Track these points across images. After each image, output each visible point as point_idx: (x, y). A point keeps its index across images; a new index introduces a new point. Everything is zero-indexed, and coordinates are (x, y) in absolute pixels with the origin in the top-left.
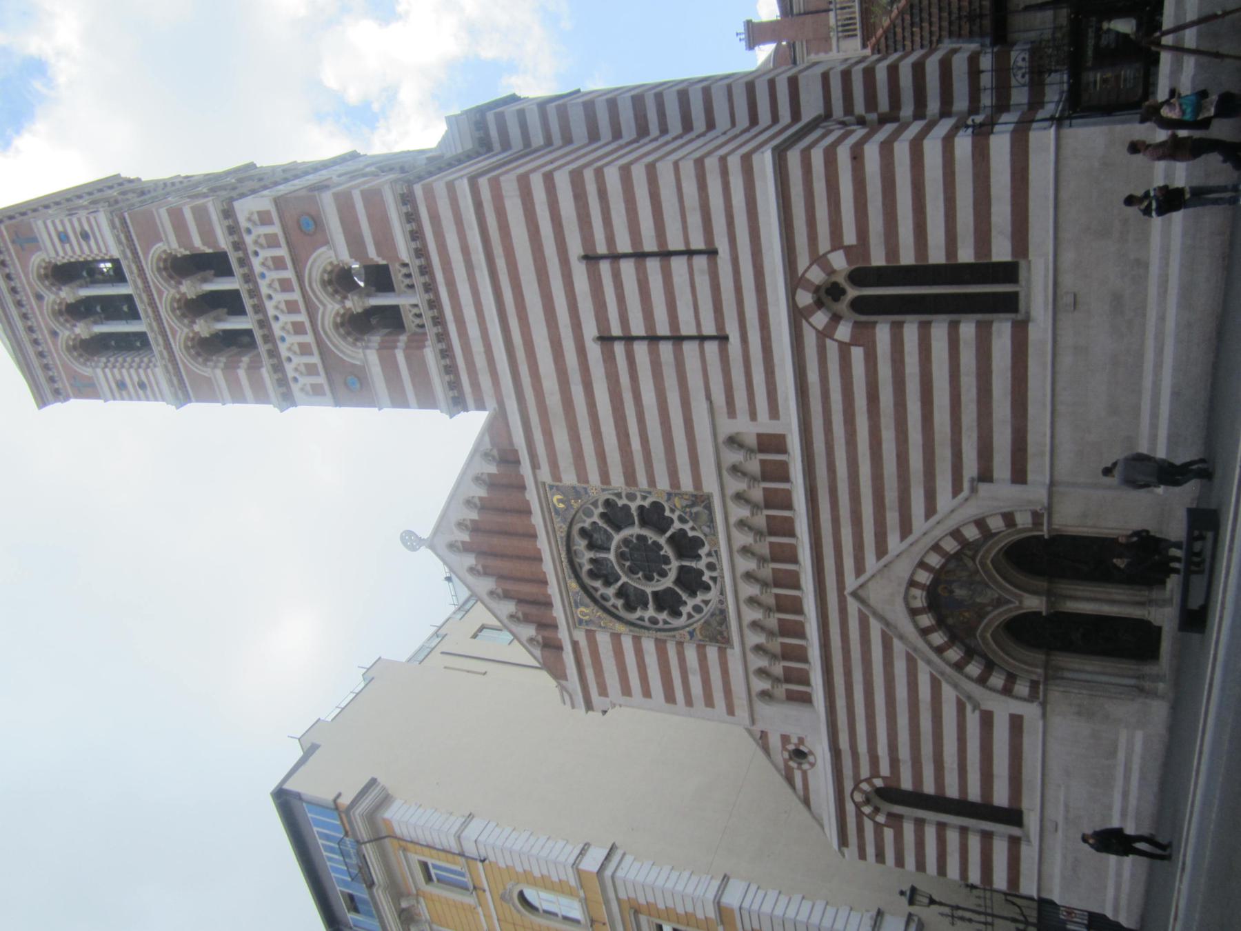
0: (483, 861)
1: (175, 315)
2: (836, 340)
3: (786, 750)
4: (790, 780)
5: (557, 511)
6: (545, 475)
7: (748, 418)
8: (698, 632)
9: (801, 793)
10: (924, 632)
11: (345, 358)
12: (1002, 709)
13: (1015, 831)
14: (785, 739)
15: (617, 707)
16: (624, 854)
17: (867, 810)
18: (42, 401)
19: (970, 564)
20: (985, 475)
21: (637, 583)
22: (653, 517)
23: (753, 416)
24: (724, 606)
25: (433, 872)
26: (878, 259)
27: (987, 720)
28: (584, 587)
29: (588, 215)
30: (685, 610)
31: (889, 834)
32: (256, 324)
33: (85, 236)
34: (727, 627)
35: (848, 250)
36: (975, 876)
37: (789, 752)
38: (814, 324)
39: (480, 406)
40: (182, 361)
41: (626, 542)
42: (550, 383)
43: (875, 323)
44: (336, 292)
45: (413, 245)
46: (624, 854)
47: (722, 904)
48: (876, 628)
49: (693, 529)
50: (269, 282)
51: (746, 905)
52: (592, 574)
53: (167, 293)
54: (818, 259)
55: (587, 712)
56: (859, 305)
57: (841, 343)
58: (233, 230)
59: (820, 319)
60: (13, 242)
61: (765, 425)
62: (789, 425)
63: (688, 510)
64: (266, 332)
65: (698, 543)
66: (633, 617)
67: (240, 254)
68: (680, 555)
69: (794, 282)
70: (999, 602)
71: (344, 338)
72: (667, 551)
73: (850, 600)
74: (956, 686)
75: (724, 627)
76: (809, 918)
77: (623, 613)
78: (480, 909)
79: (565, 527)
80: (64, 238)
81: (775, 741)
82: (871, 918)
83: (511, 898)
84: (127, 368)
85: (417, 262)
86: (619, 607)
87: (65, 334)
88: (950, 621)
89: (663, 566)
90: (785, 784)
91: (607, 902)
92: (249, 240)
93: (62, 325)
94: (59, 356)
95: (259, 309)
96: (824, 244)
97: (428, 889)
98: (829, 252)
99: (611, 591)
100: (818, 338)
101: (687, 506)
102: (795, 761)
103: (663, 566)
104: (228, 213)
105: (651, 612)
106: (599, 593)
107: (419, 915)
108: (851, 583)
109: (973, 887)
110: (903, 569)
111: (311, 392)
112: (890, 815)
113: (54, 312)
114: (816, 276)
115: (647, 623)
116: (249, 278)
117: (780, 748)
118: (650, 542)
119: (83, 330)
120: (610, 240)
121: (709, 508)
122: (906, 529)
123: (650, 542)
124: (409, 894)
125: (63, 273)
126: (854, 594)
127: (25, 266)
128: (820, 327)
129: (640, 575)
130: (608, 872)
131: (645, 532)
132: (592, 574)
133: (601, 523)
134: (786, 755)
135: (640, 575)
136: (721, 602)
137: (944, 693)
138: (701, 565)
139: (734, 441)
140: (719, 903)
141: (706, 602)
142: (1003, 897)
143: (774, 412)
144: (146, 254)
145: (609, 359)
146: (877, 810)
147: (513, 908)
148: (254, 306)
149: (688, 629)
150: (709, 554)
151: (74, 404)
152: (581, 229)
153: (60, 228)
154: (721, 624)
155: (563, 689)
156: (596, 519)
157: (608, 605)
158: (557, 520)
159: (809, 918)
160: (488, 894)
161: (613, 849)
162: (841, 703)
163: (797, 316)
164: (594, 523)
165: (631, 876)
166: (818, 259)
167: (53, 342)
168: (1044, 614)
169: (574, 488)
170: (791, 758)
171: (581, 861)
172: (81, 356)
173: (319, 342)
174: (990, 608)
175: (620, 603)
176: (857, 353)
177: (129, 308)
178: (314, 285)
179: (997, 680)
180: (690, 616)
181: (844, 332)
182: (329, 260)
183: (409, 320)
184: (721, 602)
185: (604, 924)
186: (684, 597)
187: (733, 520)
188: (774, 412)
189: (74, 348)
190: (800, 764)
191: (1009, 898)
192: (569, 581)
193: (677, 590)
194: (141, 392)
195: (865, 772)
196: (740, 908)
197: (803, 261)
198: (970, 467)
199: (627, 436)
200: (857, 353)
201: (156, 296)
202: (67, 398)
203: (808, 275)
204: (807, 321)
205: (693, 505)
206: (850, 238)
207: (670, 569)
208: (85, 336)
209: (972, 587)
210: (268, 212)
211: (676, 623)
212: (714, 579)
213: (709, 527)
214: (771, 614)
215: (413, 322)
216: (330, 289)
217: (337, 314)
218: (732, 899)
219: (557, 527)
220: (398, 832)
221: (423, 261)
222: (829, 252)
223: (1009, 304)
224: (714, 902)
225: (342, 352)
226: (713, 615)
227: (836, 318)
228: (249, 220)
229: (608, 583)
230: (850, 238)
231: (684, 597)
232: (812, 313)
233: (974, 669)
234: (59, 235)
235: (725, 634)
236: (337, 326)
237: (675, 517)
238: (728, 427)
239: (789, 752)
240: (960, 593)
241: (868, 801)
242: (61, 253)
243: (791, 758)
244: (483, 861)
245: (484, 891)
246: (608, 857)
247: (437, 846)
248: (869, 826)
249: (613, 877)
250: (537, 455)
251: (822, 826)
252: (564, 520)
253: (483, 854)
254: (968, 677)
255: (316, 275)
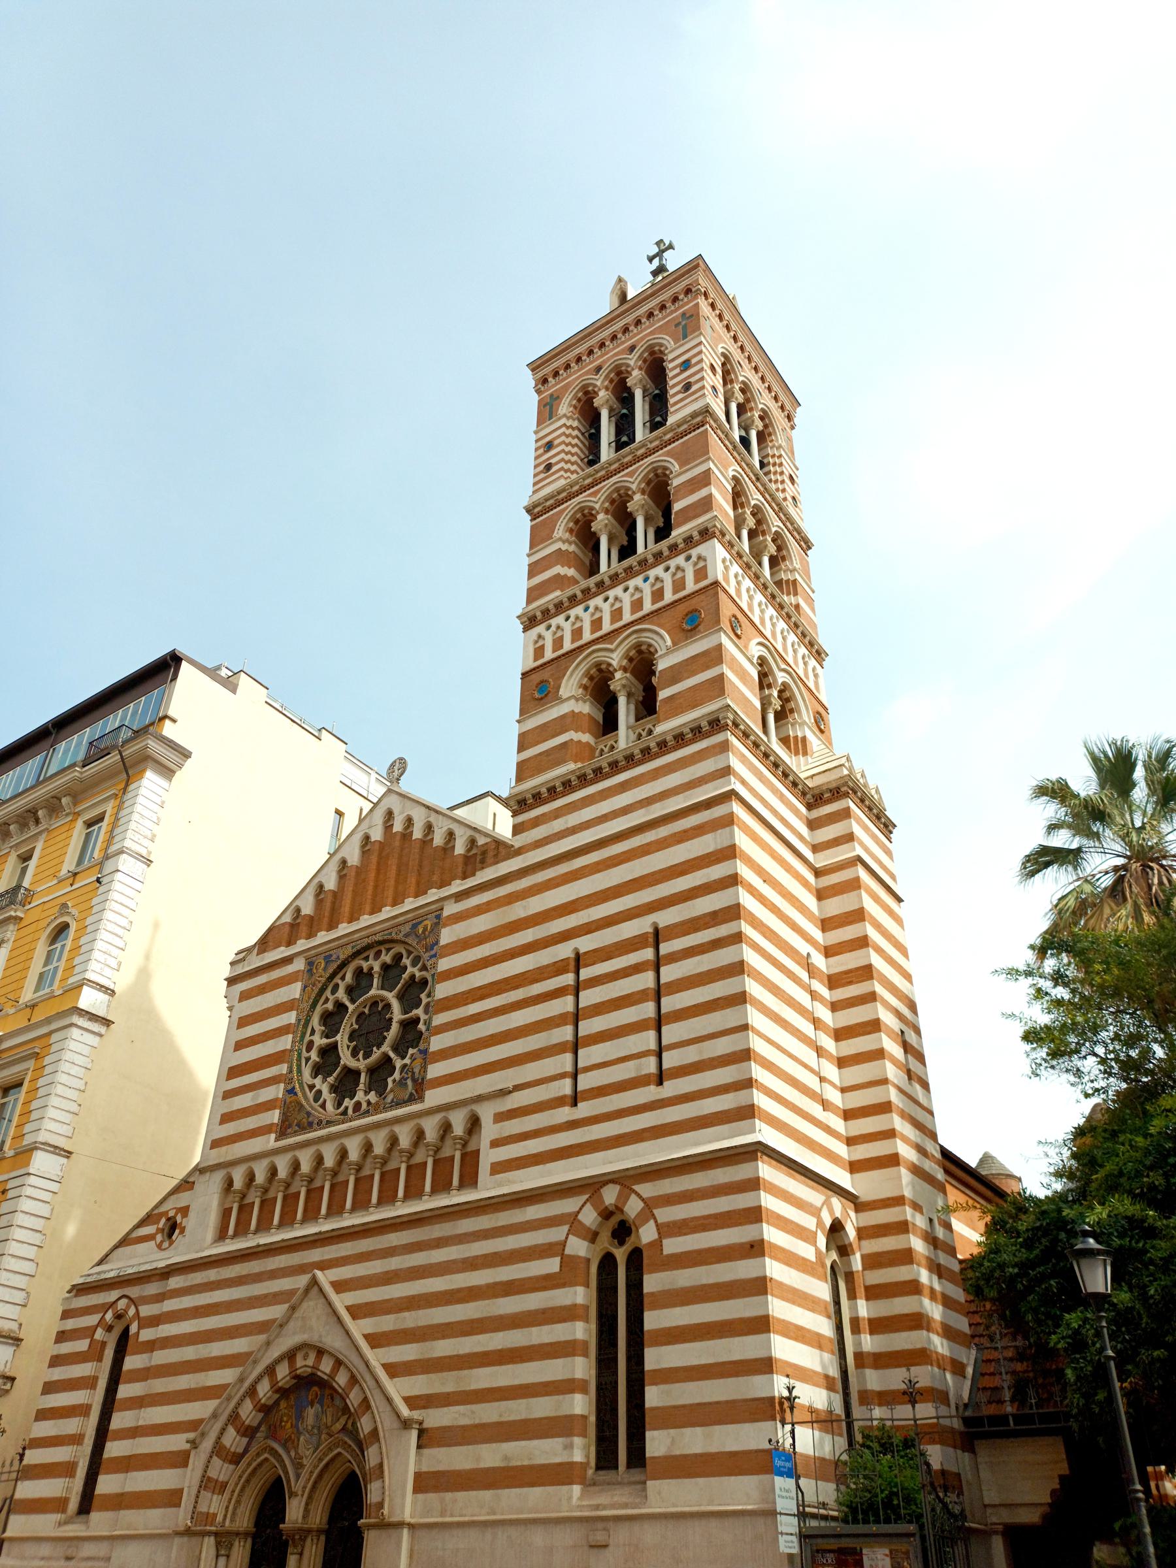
0: (98, 881)
1: (612, 492)
2: (567, 1238)
3: (176, 1214)
4: (142, 1223)
5: (415, 926)
6: (450, 909)
7: (493, 1137)
8: (294, 1098)
9: (134, 1235)
10: (270, 1371)
11: (566, 677)
12: (186, 1479)
13: (73, 1505)
14: (185, 1211)
15: (228, 1013)
16: (101, 1035)
17: (109, 1316)
18: (535, 367)
19: (338, 1426)
20: (426, 1438)
21: (348, 1024)
22: (411, 1034)
23: (495, 1144)
24: (315, 1126)
25: (96, 827)
26: (652, 1283)
27: (180, 1460)
28: (344, 965)
29: (697, 930)
30: (318, 1081)
31: (82, 1345)
32: (642, 557)
33: (687, 387)
34: (120, 807)
35: (657, 1244)
36: (34, 1457)
37: (174, 1217)
38: (584, 1208)
39: (517, 830)
40: (567, 507)
41: (388, 1006)
42: (536, 904)
43: (587, 1286)
44: (631, 660)
45: (686, 730)
46: (101, 1035)
47: (35, 1152)
48: (275, 1312)
49: (394, 1081)
50: (600, 606)
51: (32, 1180)
52: (359, 972)
53: (634, 480)
54: (650, 1205)
55: (225, 980)
56: (607, 1263)
57: (563, 1244)
58: (689, 542)
59: (589, 1217)
60: (684, 314)
61: (489, 1157)
62: (489, 1187)
63: (410, 1074)
64: (553, 611)
65: (381, 1089)
66: (315, 1021)
67: (666, 553)
68: (372, 1071)
69: (626, 1180)
70: (299, 1466)
71: (587, 674)
72: (377, 1054)
73: (302, 1281)
74: (215, 1416)
75: (297, 1128)
76: (13, 1256)
77: (319, 1009)
78: (55, 882)
79: (400, 937)
80: (686, 365)
81: (183, 1199)
82: (11, 1331)
83: (62, 915)
84: (569, 447)
85: (653, 745)
86: (325, 1006)
87: (633, 360)
88: (283, 1404)
89: (362, 1052)
90: (142, 1213)
91: (48, 1021)
92: (680, 560)
93: (607, 376)
94: (575, 378)
95: (659, 557)
96: (665, 1214)
97: (80, 824)
98: (656, 1222)
99: (341, 994)
100: (569, 1214)
101: (413, 1073)
102: (164, 1224)
103: (362, 1052)
104: (706, 534)
105: (319, 1041)
106: (340, 982)
107: (57, 817)
108: (324, 1278)
109: (22, 1456)
110: (334, 1341)
111: (537, 646)
112: (104, 1344)
113: (651, 346)
114: (633, 1207)
115: (307, 1038)
116: (615, 579)
117: (179, 1206)
118: (385, 1034)
119: (603, 398)
120: (674, 957)
121: (411, 1099)
122: (375, 1340)
123: (385, 1034)
124: (75, 804)
125: (656, 369)
126: (314, 1282)
127: (661, 329)
128: (580, 1217)
129: (356, 1027)
130: (76, 1019)
131: (395, 1027)
132: (359, 972)
133: (405, 976)
134: (171, 1214)
135: (356, 1027)
136: (320, 1123)
137: (212, 1401)
138: (360, 1096)
139: (474, 1123)
140: (36, 1148)
141: (323, 1106)
142: (9, 1495)
143: (499, 1168)
144: (668, 454)
145: (558, 968)
146: (109, 1329)
147: (53, 917)
148: (631, 567)
149: (297, 1086)
150: (369, 1103)
151: (532, 401)
152: (683, 923)
153: (556, 442)
154: (298, 1125)
155: (248, 950)
156: (410, 970)
157: (328, 993)
158: (407, 928)
159: (13, 1256)
160: (70, 889)
161: (107, 1022)
162: (212, 1275)
163: (591, 1187)
164: (405, 968)
165: (72, 1045)
166: (650, 1205)
167: (623, 350)
168: (281, 1526)
169: (437, 943)
170: (168, 1219)
171: (92, 987)
172: (579, 400)
173: (581, 649)
174: (293, 1454)
175: (330, 1006)
176: (552, 1265)
177: (624, 442)
178: (634, 636)
179: (220, 1470)
180: (312, 1087)
181: (578, 1247)
182: (658, 649)
183: (609, 740)
184: (320, 1123)
185: (29, 1020)
186: (331, 1079)
187: (397, 1129)
188: (499, 1168)
189: (652, 353)
190: (163, 1230)
191: (8, 1501)
192: (349, 947)
193: (339, 1069)
194: (542, 467)
195: (146, 1311)
196: (29, 1174)
197: (647, 1189)
198: (435, 1418)
199: (482, 998)
200: (552, 1265)
201: (592, 490)
202: (538, 392)
203: (633, 1197)
204: (587, 1200)
205: (414, 1080)
206: (672, 1246)
207: (358, 1060)
208: (630, 382)
209: (316, 1431)
210: (706, 577)
211: (307, 1072)
212: (345, 1113)
213: (392, 1101)
214: (305, 1183)
215: (643, 730)
216: (632, 653)
217: (610, 665)
218: (42, 1162)
219: (402, 928)
220: (132, 787)
221: (671, 743)
222: (656, 1222)
223: (606, 1458)
224: (36, 1142)
225: (571, 675)
226: (309, 1114)
227: (593, 1237)
228: (699, 558)
229: (350, 991)
230: (672, 1246)
231: (331, 1079)
232: (595, 1207)
233: (231, 1439)
234: (687, 361)
235: (289, 1131)
236: (598, 665)
237: (407, 1061)
238: (486, 1113)
239: (174, 1217)
240: (311, 1413)
241: (119, 1317)
242: (671, 366)
243: (168, 1219)
244: (98, 881)
245: (72, 885)
246: (93, 1017)
247: (116, 831)
248: (92, 1320)
249: (72, 1025)
250: (468, 897)
251: (100, 1263)
252: (406, 935)
253: (104, 880)
254: (223, 1431)
255: (646, 638)
